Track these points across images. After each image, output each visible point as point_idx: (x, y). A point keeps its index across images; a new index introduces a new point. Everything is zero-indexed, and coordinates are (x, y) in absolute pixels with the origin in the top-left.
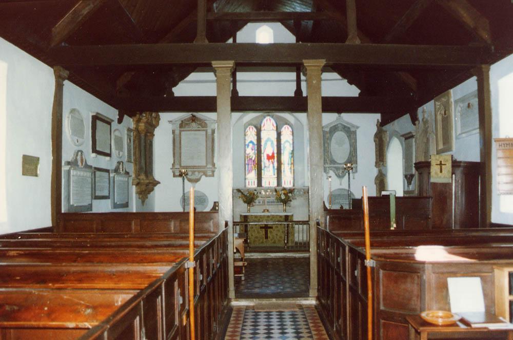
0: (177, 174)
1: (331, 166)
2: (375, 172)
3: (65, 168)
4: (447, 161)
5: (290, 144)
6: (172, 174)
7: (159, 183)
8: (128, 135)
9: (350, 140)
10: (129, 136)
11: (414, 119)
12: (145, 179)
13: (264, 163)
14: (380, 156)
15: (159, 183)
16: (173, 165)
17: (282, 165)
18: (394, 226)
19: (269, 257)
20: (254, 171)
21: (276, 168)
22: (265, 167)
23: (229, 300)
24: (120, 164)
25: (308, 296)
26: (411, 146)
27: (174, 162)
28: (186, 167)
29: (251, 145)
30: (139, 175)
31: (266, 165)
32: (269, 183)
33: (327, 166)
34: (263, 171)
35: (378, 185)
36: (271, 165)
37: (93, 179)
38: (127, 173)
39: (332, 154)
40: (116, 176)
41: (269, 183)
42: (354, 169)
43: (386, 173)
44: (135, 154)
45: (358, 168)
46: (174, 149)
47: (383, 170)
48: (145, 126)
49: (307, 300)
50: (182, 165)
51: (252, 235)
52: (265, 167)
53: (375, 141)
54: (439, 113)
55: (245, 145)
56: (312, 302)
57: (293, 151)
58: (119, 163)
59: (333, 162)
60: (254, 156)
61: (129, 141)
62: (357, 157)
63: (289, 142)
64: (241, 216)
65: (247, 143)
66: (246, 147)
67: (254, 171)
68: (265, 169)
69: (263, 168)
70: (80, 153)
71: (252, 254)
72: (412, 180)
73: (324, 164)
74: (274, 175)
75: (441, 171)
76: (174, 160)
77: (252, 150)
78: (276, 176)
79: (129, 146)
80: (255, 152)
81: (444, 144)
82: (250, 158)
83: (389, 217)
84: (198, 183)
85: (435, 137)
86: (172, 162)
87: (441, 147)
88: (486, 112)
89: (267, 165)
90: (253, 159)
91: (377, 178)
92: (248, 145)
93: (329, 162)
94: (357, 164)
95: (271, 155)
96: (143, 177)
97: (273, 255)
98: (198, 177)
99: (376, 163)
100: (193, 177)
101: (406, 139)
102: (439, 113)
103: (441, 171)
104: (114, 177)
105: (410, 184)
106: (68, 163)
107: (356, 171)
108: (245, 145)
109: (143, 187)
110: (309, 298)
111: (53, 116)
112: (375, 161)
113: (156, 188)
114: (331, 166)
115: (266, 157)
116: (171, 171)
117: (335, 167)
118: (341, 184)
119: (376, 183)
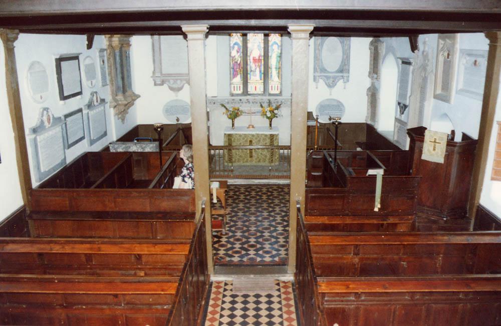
0: (158, 82)
1: (321, 74)
2: (368, 83)
3: (29, 138)
4: (442, 140)
5: (279, 46)
6: (153, 82)
7: (140, 96)
8: (100, 57)
9: (343, 47)
10: (101, 57)
11: (414, 47)
12: (123, 99)
13: (251, 67)
14: (374, 67)
15: (138, 96)
16: (154, 72)
17: (270, 69)
18: (377, 207)
19: (253, 183)
20: (239, 76)
21: (262, 72)
22: (251, 71)
23: (208, 276)
24: (93, 96)
25: (286, 272)
26: (407, 74)
27: (154, 70)
28: (170, 75)
29: (236, 47)
30: (116, 95)
31: (253, 69)
32: (256, 87)
33: (317, 74)
34: (249, 76)
35: (369, 96)
36: (258, 70)
37: (64, 129)
38: (103, 101)
39: (323, 62)
40: (90, 112)
41: (256, 87)
42: (345, 78)
43: (380, 88)
44: (110, 74)
45: (350, 76)
46: (154, 56)
47: (376, 84)
48: (120, 41)
49: (285, 276)
50: (163, 73)
51: (236, 154)
52: (251, 71)
53: (370, 49)
54: (441, 54)
55: (230, 47)
56: (289, 277)
57: (281, 53)
58: (92, 94)
59: (323, 70)
60: (240, 59)
61: (102, 63)
62: (349, 66)
63: (277, 44)
64: (225, 134)
65: (232, 45)
66: (231, 49)
67: (239, 76)
68: (252, 73)
69: (249, 72)
70: (45, 112)
71: (237, 180)
72: (405, 110)
73: (314, 73)
74: (261, 79)
75: (434, 149)
76: (154, 68)
77: (238, 52)
78: (262, 81)
79: (102, 69)
80: (240, 54)
81: (443, 89)
82: (236, 60)
83: (374, 197)
84: (180, 92)
85: (434, 77)
86: (153, 69)
87: (439, 91)
88: (493, 86)
89: (253, 69)
90: (239, 62)
91: (369, 89)
92: (233, 48)
93: (318, 70)
94: (349, 73)
95: (257, 58)
96: (120, 97)
97: (256, 181)
98: (180, 86)
99: (370, 73)
100: (175, 86)
101: (403, 63)
102: (441, 54)
103: (434, 149)
104: (88, 113)
105: (403, 113)
106: (35, 131)
107: (348, 81)
108: (230, 47)
109: (122, 108)
110: (286, 275)
111: (7, 87)
112: (369, 70)
113: (137, 102)
114: (321, 74)
115: (252, 61)
116: (152, 79)
117: (325, 76)
118: (331, 95)
119: (367, 95)
